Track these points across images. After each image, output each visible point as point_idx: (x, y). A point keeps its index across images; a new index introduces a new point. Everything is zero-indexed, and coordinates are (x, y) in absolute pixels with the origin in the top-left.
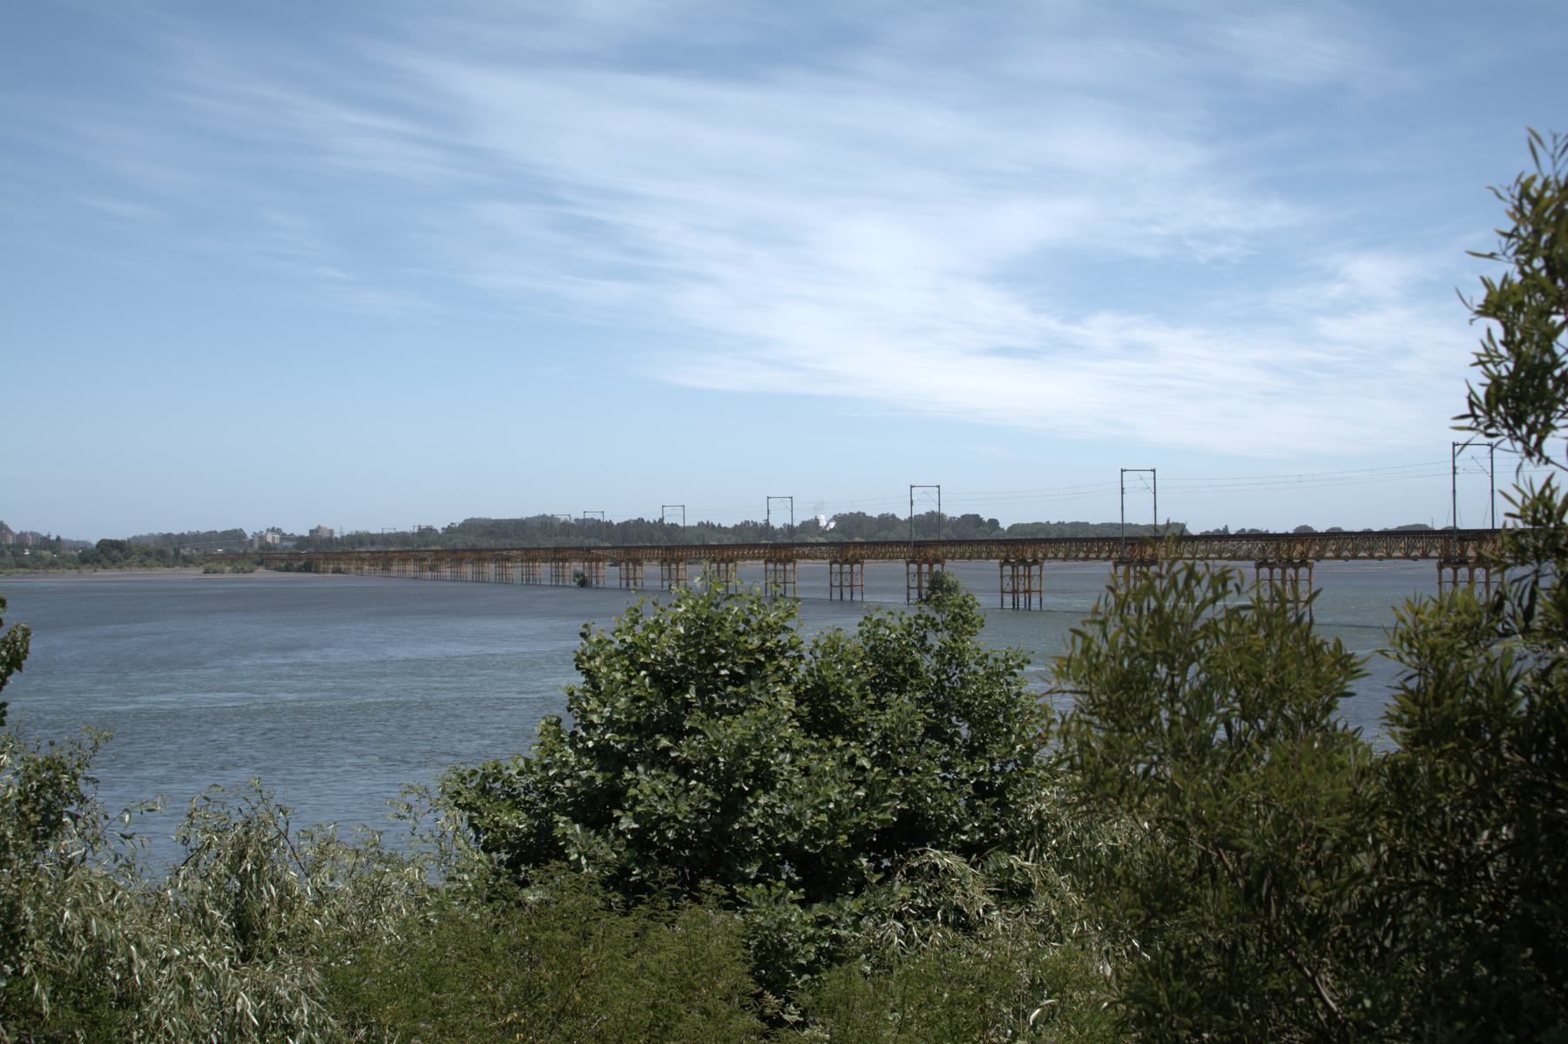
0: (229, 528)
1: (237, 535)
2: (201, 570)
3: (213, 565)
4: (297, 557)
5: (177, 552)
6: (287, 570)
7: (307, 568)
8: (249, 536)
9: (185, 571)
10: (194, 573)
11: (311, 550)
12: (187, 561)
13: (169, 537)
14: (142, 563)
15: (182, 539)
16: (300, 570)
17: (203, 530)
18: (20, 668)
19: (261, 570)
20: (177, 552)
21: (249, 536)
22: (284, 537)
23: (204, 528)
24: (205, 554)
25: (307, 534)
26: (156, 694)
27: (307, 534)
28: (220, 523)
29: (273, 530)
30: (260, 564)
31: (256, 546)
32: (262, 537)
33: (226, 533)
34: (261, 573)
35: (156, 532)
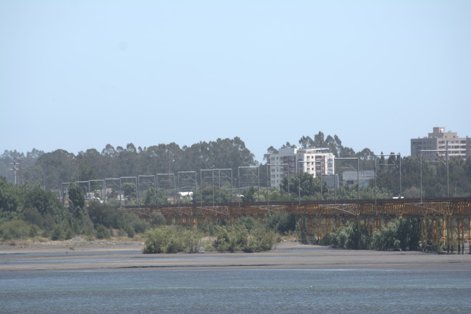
0: (210, 137)
1: (229, 153)
2: (140, 245)
3: (167, 232)
4: (382, 209)
5: (76, 197)
6: (356, 243)
7: (407, 239)
8: (260, 159)
9: (100, 246)
10: (120, 252)
11: (416, 191)
12: (104, 222)
13: (57, 159)
14: (256, 251)
15: (92, 166)
16: (386, 244)
17: (144, 140)
18: (304, 137)
19: (290, 243)
20: (76, 197)
21: (260, 159)
22: (348, 159)
23: (145, 139)
24: (149, 205)
25: (405, 151)
26: (124, 251)
27: (405, 151)
28: (188, 126)
29: (320, 141)
30: (286, 228)
31: (276, 182)
32: (290, 161)
33: (201, 147)
34: (290, 252)
35: (24, 149)
